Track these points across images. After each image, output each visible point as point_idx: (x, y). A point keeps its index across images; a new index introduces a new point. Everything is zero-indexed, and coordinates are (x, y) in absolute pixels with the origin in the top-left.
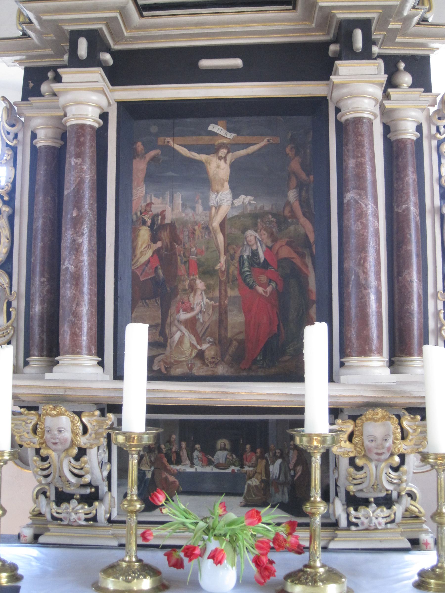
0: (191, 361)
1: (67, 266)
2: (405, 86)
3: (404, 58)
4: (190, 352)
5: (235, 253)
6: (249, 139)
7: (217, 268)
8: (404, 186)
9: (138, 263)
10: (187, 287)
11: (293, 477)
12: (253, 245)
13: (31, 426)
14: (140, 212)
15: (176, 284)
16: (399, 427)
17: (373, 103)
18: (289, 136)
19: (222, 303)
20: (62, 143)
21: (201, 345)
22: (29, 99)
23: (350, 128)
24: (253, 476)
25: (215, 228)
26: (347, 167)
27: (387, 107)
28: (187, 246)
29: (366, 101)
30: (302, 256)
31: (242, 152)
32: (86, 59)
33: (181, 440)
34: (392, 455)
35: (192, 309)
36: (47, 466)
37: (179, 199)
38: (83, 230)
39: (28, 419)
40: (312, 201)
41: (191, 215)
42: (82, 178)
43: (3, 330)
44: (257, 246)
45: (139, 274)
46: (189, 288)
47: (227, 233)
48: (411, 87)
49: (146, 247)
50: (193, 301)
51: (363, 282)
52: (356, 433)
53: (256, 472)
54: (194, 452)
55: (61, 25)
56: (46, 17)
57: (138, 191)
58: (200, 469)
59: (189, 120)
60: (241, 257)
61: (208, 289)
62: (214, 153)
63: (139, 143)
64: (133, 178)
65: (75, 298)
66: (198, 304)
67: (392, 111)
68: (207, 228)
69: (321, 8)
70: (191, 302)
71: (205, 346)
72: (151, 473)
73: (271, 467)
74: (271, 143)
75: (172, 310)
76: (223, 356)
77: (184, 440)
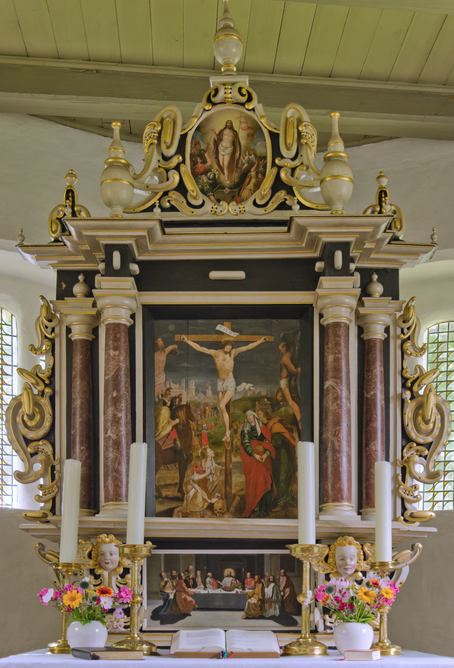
0: (203, 512)
1: (110, 434)
2: (377, 295)
3: (377, 271)
4: (202, 505)
5: (238, 428)
6: (249, 338)
7: (223, 440)
8: (372, 377)
9: (160, 436)
10: (200, 455)
11: (283, 597)
12: (252, 422)
13: (87, 552)
14: (162, 395)
15: (191, 452)
16: (362, 551)
17: (349, 310)
18: (282, 335)
19: (228, 467)
20: (94, 337)
21: (211, 499)
22: (65, 298)
23: (331, 331)
24: (252, 596)
25: (222, 409)
26: (327, 361)
27: (361, 312)
28: (199, 422)
29: (344, 309)
30: (291, 431)
31: (244, 348)
32: (120, 269)
33: (196, 569)
34: (356, 571)
35: (204, 472)
36: (100, 582)
37: (192, 385)
38: (122, 407)
39: (84, 548)
40: (299, 388)
41: (202, 398)
42: (119, 367)
43: (48, 489)
44: (255, 423)
45: (161, 445)
46: (201, 455)
47: (231, 412)
48: (381, 296)
49: (166, 423)
50: (205, 465)
51: (338, 448)
52: (330, 555)
53: (254, 594)
54: (207, 578)
55: (98, 240)
56: (86, 233)
57: (159, 378)
58: (211, 591)
59: (200, 321)
60: (243, 431)
61: (217, 456)
62: (221, 349)
63: (160, 339)
64: (155, 368)
65: (117, 459)
66: (208, 468)
67: (365, 315)
68: (215, 408)
69: (310, 233)
70: (203, 466)
71: (214, 500)
72: (173, 594)
73: (266, 590)
74: (267, 341)
75: (188, 472)
76: (228, 508)
77: (199, 570)
